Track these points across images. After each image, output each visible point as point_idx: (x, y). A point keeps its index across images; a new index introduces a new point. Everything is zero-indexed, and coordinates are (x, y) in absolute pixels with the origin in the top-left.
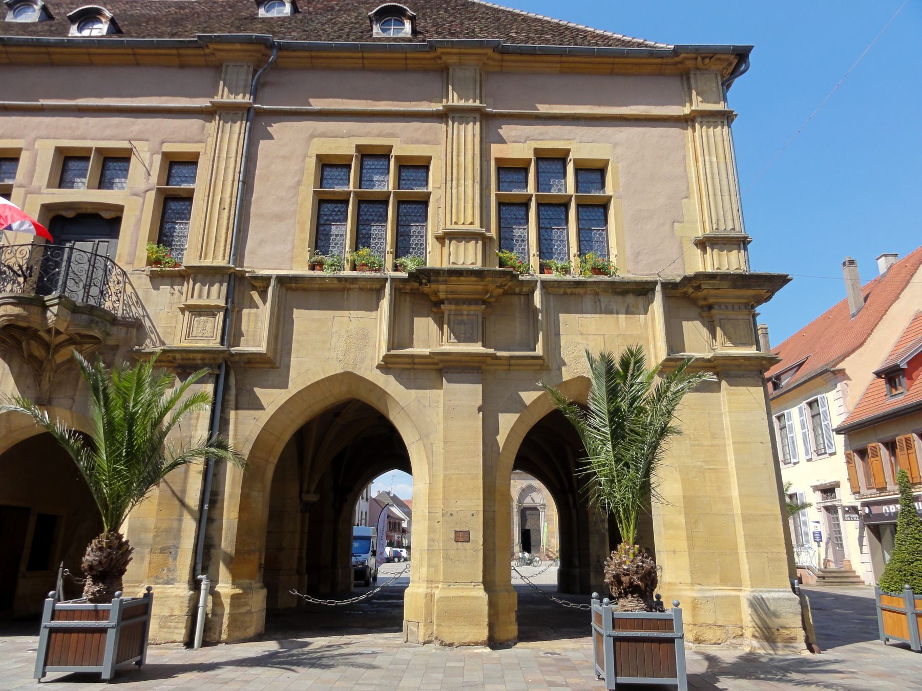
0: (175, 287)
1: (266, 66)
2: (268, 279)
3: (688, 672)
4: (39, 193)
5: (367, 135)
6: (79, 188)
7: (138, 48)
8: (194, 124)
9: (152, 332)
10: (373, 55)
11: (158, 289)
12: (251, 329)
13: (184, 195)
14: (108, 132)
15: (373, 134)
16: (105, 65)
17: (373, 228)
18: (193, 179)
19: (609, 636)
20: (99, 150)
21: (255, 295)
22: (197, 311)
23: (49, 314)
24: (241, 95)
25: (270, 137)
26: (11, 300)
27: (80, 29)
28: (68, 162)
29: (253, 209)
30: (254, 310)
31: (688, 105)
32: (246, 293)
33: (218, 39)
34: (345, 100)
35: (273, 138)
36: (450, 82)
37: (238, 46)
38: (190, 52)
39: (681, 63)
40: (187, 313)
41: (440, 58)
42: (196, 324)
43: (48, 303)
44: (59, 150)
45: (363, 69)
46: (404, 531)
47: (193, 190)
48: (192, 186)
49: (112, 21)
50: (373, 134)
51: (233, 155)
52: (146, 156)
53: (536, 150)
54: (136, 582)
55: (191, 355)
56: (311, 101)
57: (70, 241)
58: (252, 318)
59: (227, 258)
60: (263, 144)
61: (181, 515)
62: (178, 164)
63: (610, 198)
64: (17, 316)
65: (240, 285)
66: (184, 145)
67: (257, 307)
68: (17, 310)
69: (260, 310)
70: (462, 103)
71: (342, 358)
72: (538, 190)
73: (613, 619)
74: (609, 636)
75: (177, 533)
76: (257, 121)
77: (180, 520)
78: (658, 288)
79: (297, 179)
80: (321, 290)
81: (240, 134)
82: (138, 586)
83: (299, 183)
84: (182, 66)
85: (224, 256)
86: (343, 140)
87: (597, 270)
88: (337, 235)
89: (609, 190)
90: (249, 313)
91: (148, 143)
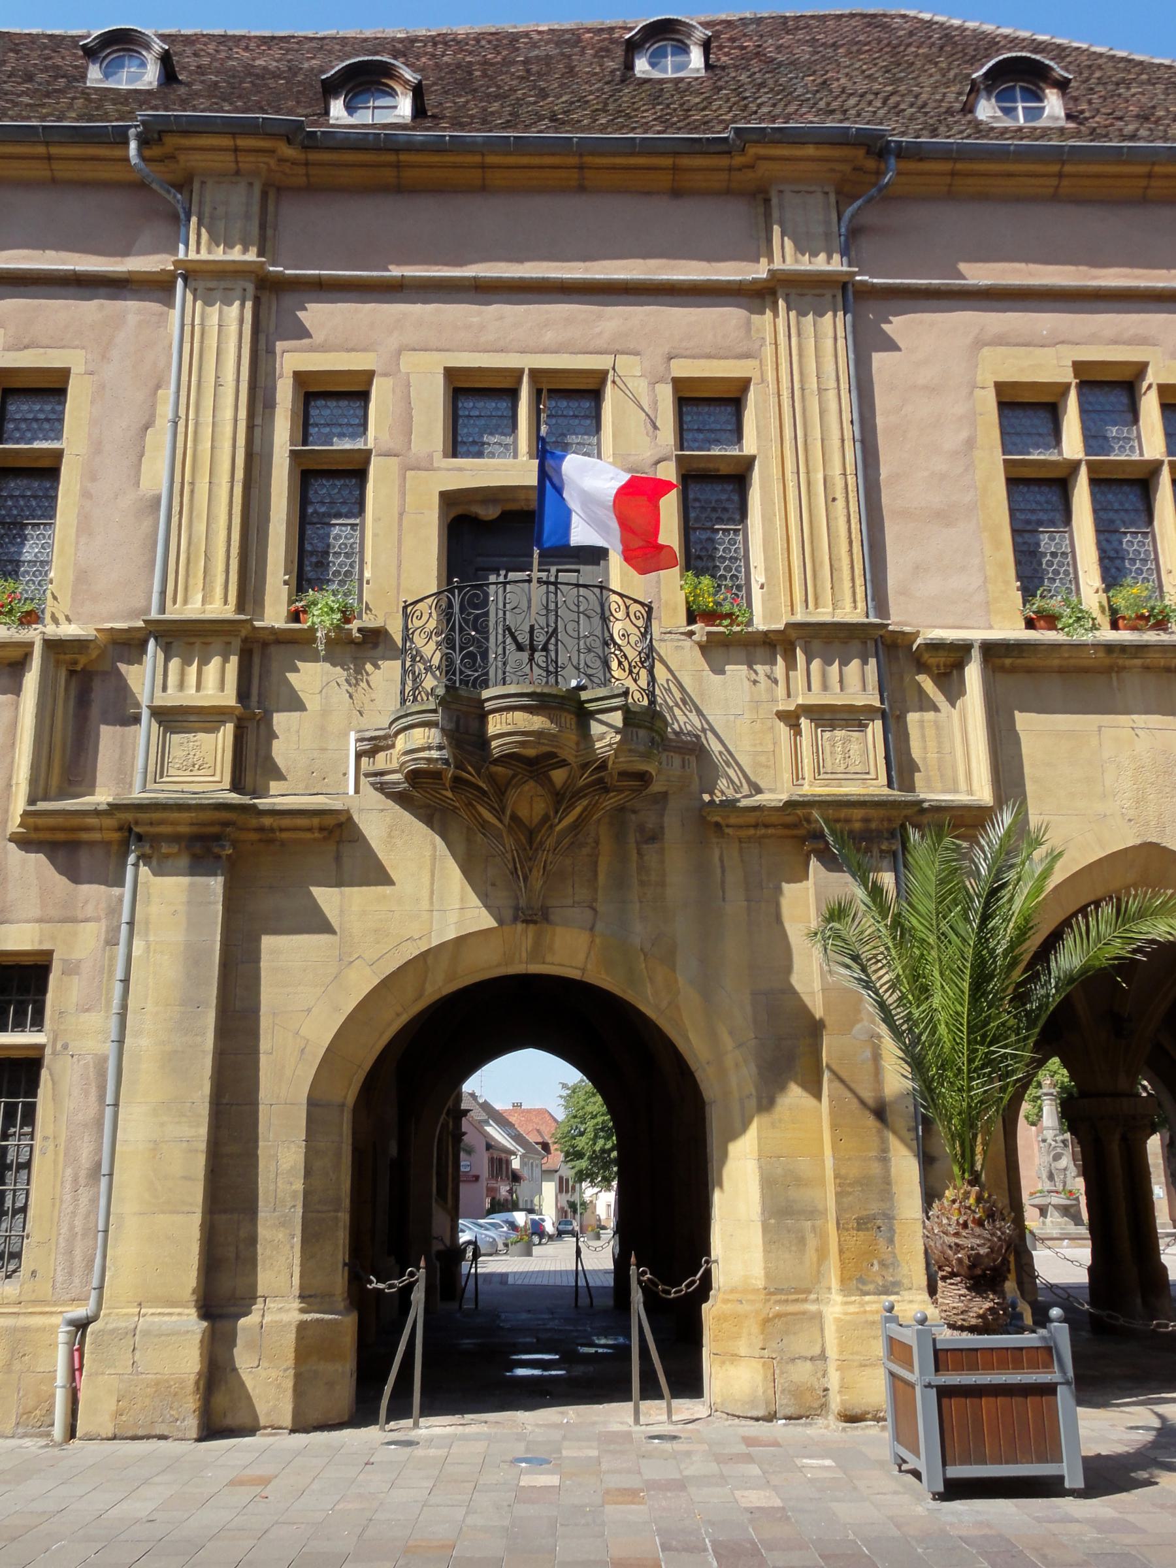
0: (758, 667)
1: (874, 191)
2: (959, 652)
3: (1083, 1454)
4: (430, 468)
5: (1092, 340)
6: (492, 455)
7: (592, 154)
8: (726, 319)
9: (728, 764)
10: (1082, 168)
11: (723, 672)
12: (932, 756)
13: (46, 463)
14: (549, 337)
15: (1106, 338)
16: (512, 190)
17: (336, 531)
18: (55, 425)
19: (929, 1386)
20: (533, 372)
21: (926, 683)
22: (828, 717)
23: (596, 728)
24: (822, 256)
25: (892, 346)
26: (525, 701)
27: (350, 108)
28: (476, 402)
29: (885, 500)
30: (930, 716)
31: (764, 261)
32: (907, 679)
33: (778, 136)
34: (1033, 267)
35: (898, 349)
36: (776, 214)
37: (810, 151)
38: (699, 161)
39: (752, 167)
40: (804, 723)
41: (172, 157)
42: (827, 745)
43: (591, 706)
44: (451, 374)
45: (1055, 198)
46: (516, 1178)
47: (58, 455)
48: (54, 445)
49: (418, 93)
50: (1106, 338)
51: (832, 384)
52: (640, 387)
53: (1078, 367)
54: (797, 1291)
55: (844, 813)
56: (963, 267)
57: (496, 571)
58: (930, 732)
59: (861, 605)
60: (879, 359)
61: (885, 1150)
62: (709, 407)
63: (751, 460)
64: (539, 734)
65: (910, 666)
66: (715, 362)
67: (936, 709)
68: (538, 722)
69: (942, 716)
70: (219, 254)
71: (1131, 813)
72: (1088, 450)
73: (936, 1352)
74: (929, 1386)
75: (885, 1187)
76: (864, 306)
77: (884, 1158)
78: (976, 654)
79: (964, 434)
80: (1062, 671)
81: (835, 339)
82: (806, 1300)
83: (970, 443)
84: (677, 193)
85: (855, 601)
86: (1047, 350)
87: (1141, 621)
88: (1054, 555)
89: (750, 445)
90: (922, 722)
91: (642, 358)
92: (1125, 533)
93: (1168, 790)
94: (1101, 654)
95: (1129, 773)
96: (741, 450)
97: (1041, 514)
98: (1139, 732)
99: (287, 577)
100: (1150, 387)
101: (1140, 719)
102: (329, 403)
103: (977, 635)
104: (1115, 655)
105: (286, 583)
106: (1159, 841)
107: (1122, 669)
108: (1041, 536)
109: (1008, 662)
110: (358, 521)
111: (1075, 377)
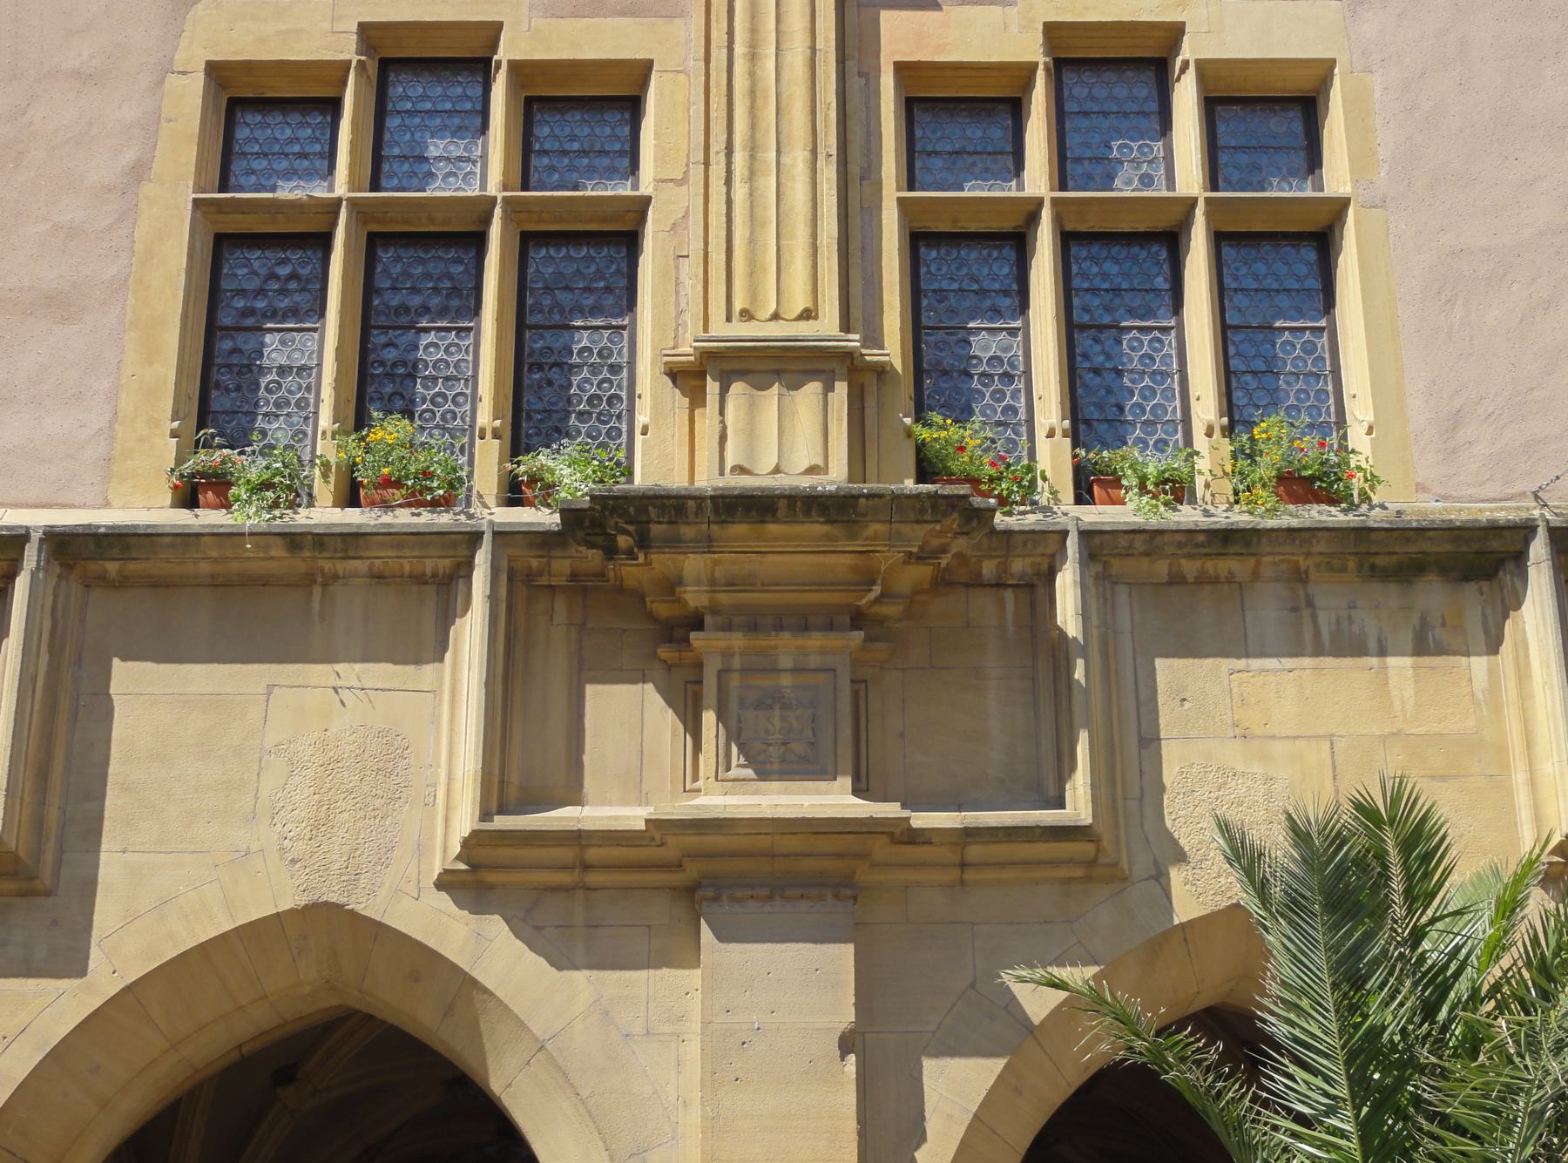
72: (1213, 182)
79: (130, 156)
80: (220, 584)
83: (139, 172)
92: (427, 330)
93: (378, 802)
94: (278, 551)
95: (310, 773)
96: (1021, 187)
97: (1089, 296)
98: (344, 694)
99: (498, 423)
100: (1186, 64)
101: (349, 672)
102: (269, 119)
103: (38, 519)
104: (307, 554)
105: (174, 434)
106: (342, 900)
107: (332, 579)
108: (268, 338)
109: (112, 567)
110: (1018, 324)
111: (1046, 55)
